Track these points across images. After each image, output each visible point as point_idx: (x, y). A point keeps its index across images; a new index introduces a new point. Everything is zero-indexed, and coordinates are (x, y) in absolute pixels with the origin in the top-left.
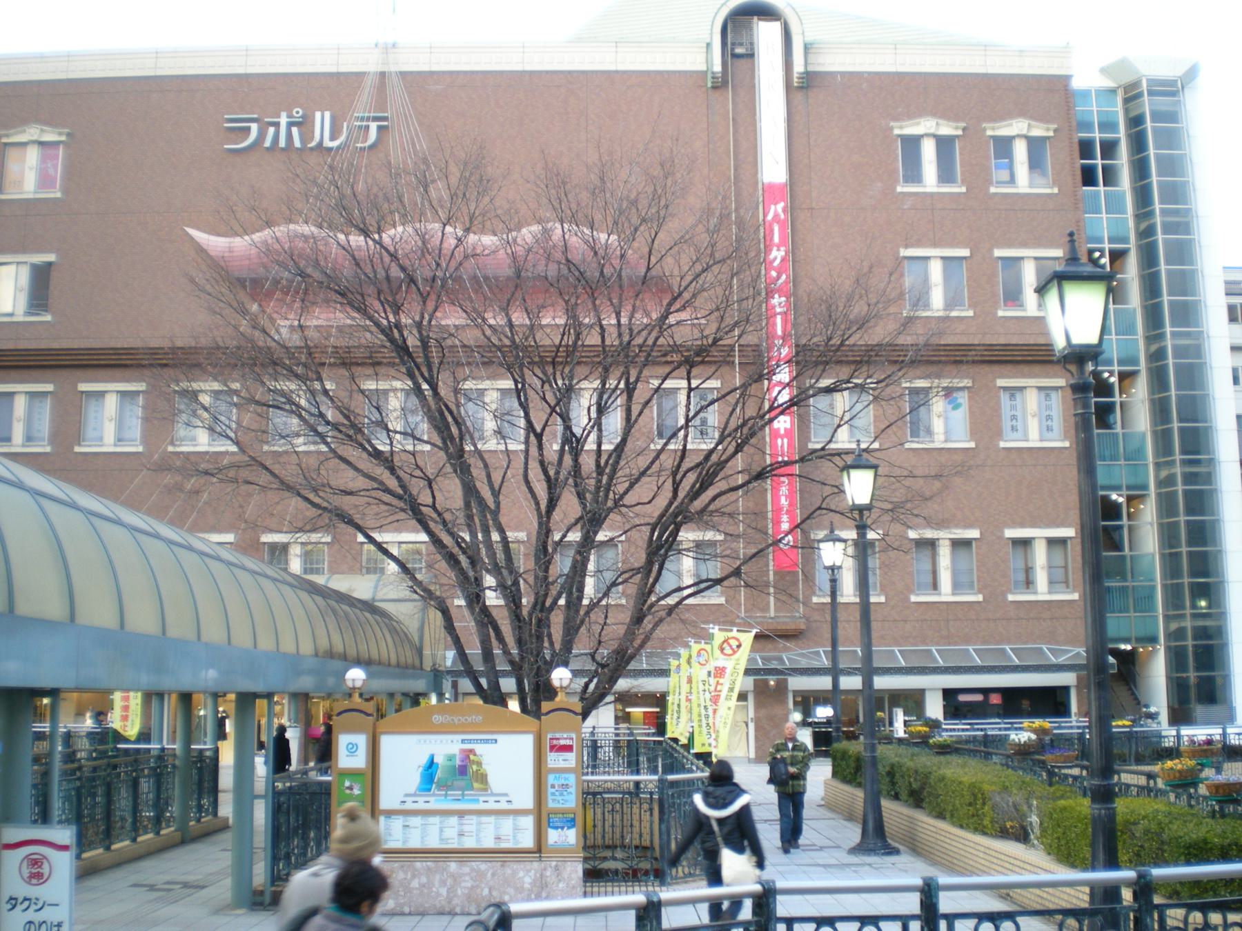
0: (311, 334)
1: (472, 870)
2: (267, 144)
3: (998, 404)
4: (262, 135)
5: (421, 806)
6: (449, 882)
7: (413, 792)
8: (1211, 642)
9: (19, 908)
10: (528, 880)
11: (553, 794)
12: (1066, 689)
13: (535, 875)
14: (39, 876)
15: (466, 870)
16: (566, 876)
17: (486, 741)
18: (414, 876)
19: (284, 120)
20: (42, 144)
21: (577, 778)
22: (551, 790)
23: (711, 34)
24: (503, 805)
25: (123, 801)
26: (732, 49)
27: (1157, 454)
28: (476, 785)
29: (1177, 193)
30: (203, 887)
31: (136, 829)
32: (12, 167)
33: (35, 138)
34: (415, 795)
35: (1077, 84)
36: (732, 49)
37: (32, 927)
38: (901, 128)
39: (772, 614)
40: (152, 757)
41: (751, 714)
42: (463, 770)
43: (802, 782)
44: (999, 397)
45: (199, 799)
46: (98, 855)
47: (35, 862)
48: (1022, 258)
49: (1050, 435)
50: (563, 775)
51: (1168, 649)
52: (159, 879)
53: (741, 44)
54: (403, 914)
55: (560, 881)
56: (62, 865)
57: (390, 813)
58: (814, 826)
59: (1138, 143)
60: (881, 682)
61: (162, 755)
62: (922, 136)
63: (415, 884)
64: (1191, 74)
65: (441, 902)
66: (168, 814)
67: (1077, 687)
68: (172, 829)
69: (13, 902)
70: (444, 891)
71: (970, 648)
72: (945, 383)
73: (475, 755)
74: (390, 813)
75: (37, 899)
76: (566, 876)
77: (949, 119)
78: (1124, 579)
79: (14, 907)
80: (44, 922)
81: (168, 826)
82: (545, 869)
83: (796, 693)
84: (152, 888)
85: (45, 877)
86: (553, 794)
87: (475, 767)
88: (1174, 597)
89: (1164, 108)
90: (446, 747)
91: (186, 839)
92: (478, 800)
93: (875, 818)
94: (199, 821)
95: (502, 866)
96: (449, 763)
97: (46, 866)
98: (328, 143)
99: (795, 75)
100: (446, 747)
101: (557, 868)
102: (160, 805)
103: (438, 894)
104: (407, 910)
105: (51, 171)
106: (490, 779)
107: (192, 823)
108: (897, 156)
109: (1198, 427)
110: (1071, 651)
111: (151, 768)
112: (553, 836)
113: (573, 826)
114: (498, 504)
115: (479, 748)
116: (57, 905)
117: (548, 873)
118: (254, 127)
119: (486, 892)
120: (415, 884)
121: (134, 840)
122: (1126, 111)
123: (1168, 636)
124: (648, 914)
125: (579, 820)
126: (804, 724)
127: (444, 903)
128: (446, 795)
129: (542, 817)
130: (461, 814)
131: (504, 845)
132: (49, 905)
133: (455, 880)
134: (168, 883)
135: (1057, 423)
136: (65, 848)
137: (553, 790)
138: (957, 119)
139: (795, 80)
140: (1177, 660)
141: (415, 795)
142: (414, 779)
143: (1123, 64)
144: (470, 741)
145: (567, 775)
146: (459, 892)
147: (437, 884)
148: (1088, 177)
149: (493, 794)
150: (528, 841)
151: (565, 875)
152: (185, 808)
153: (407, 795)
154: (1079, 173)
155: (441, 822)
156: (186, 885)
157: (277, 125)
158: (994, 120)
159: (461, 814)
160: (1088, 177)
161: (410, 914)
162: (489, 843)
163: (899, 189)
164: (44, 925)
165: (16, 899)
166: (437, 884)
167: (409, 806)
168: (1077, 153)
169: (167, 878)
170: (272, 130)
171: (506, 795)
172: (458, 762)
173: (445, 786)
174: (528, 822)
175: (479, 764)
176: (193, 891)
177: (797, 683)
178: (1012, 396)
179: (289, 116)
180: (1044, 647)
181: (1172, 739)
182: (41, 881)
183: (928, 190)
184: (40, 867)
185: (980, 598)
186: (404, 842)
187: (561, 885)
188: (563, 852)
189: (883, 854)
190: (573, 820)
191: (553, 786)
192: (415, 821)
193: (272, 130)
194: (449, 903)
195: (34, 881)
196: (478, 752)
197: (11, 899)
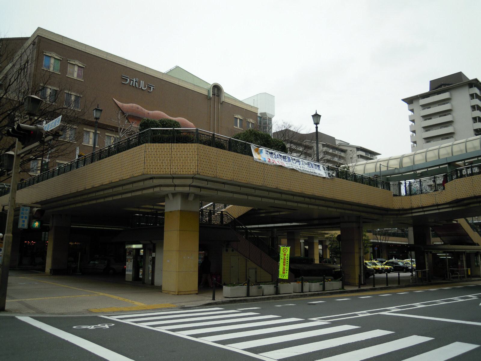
4: (130, 82)
19: (134, 80)
35: (335, 138)
43: (32, 132)
48: (90, 132)
64: (403, 100)
72: (271, 151)
74: (472, 218)
98: (143, 89)
105: (80, 74)
157: (133, 81)
170: (132, 82)
179: (136, 80)
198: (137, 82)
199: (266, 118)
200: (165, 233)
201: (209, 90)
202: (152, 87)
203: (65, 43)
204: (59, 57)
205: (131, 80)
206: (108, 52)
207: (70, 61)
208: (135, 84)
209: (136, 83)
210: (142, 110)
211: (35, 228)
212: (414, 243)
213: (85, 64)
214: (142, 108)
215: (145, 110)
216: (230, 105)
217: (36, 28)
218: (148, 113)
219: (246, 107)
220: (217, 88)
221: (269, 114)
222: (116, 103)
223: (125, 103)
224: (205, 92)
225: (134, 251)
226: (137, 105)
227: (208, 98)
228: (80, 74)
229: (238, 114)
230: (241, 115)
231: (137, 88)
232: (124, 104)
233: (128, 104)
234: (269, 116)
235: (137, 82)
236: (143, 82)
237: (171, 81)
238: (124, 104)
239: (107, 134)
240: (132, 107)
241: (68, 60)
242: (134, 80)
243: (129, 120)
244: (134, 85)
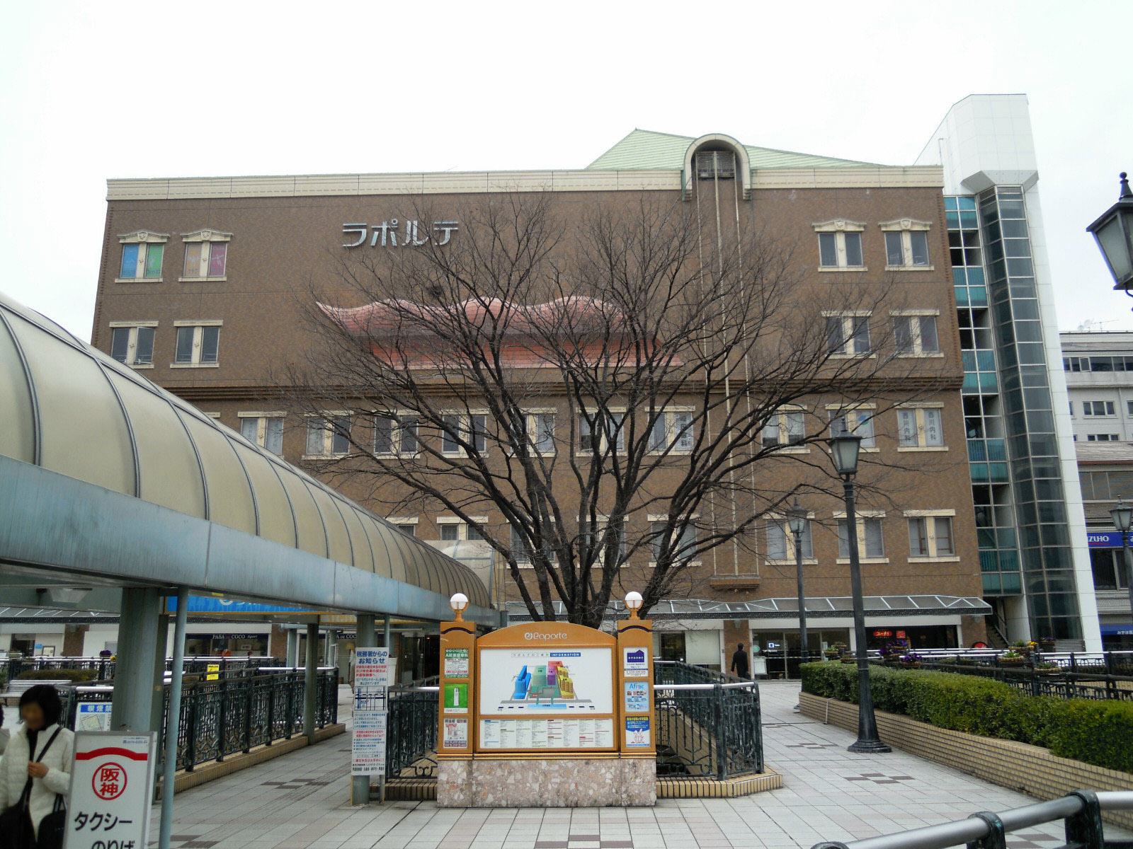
0: (398, 439)
1: (561, 767)
2: (373, 243)
3: (896, 419)
5: (516, 711)
6: (541, 778)
7: (509, 699)
8: (1061, 593)
9: (88, 826)
10: (609, 776)
11: (629, 700)
12: (954, 627)
13: (615, 771)
14: (113, 789)
15: (556, 767)
16: (642, 773)
17: (571, 655)
18: (510, 773)
19: (384, 227)
20: (212, 243)
21: (650, 688)
22: (627, 697)
23: (684, 164)
24: (587, 711)
25: (260, 712)
26: (699, 175)
27: (1013, 454)
28: (563, 693)
29: (1025, 267)
30: (326, 784)
31: (271, 734)
32: (190, 258)
33: (909, 228)
34: (510, 702)
36: (699, 175)
37: (101, 847)
38: (820, 226)
39: (737, 574)
40: (287, 675)
41: (722, 647)
42: (551, 680)
44: (896, 416)
45: (322, 710)
46: (237, 757)
47: (108, 774)
49: (933, 442)
50: (638, 684)
51: (1029, 597)
52: (287, 778)
53: (705, 171)
54: (500, 807)
55: (636, 777)
56: (139, 776)
57: (488, 718)
58: (803, 728)
59: (993, 232)
60: (811, 623)
61: (293, 675)
62: (835, 232)
63: (511, 780)
64: (1035, 178)
65: (533, 797)
66: (298, 722)
67: (962, 626)
68: (301, 734)
69: (83, 819)
70: (536, 787)
71: (882, 597)
73: (562, 666)
74: (488, 718)
75: (109, 815)
76: (642, 773)
77: (854, 220)
78: (993, 545)
79: (83, 824)
80: (115, 842)
81: (297, 732)
82: (624, 767)
83: (755, 631)
84: (281, 786)
85: (120, 790)
86: (629, 700)
87: (562, 677)
88: (1033, 559)
89: (1011, 207)
90: (537, 661)
91: (311, 741)
92: (565, 706)
93: (870, 721)
94: (321, 727)
95: (587, 763)
96: (541, 674)
97: (121, 777)
99: (744, 191)
100: (537, 661)
101: (634, 765)
102: (290, 716)
103: (532, 790)
104: (504, 803)
105: (219, 262)
106: (575, 688)
107: (316, 729)
108: (818, 246)
109: (1032, 443)
110: (956, 599)
111: (284, 685)
112: (630, 737)
113: (647, 728)
114: (549, 482)
115: (565, 661)
116: (130, 822)
117: (627, 770)
118: (364, 231)
119: (573, 786)
120: (511, 780)
121: (269, 744)
122: (982, 211)
123: (1029, 588)
124: (2, 651)
125: (652, 722)
126: (761, 654)
127: (537, 797)
128: (537, 702)
129: (620, 721)
130: (551, 718)
131: (587, 745)
132: (121, 822)
133: (546, 776)
134: (295, 781)
135: (938, 433)
136: (143, 757)
137: (630, 697)
138: (859, 219)
139: (744, 195)
140: (1038, 606)
141: (510, 702)
142: (510, 688)
143: (980, 176)
144: (558, 655)
145: (641, 684)
146: (550, 787)
147: (530, 779)
148: (956, 258)
149: (578, 701)
150: (608, 742)
151: (641, 772)
152: (311, 718)
153: (503, 702)
154: (949, 255)
155: (534, 727)
156: (311, 782)
157: (380, 230)
158: (186, 230)
159: (551, 718)
160: (956, 258)
161: (507, 807)
162: (575, 744)
163: (820, 270)
164: (114, 845)
165: (86, 816)
166: (530, 779)
167: (506, 711)
168: (947, 242)
169: (297, 776)
171: (589, 701)
172: (547, 673)
173: (537, 694)
174: (608, 725)
175: (566, 674)
176: (317, 787)
177: (755, 624)
178: (905, 415)
179: (388, 224)
180: (936, 596)
181: (1067, 661)
182: (115, 794)
183: (841, 270)
184: (115, 778)
185: (887, 560)
186: (502, 741)
187: (638, 780)
188: (639, 753)
189: (879, 751)
190: (648, 722)
191: (629, 694)
192: (511, 725)
193: (376, 233)
194: (541, 797)
195: (107, 795)
196: (564, 664)
197: (81, 815)
202: (448, 230)
203: (176, 193)
204: (158, 236)
208: (389, 238)
213: (229, 231)
216: (793, 196)
219: (900, 178)
224: (668, 181)
229: (828, 217)
239: (240, 414)
241: (880, 226)
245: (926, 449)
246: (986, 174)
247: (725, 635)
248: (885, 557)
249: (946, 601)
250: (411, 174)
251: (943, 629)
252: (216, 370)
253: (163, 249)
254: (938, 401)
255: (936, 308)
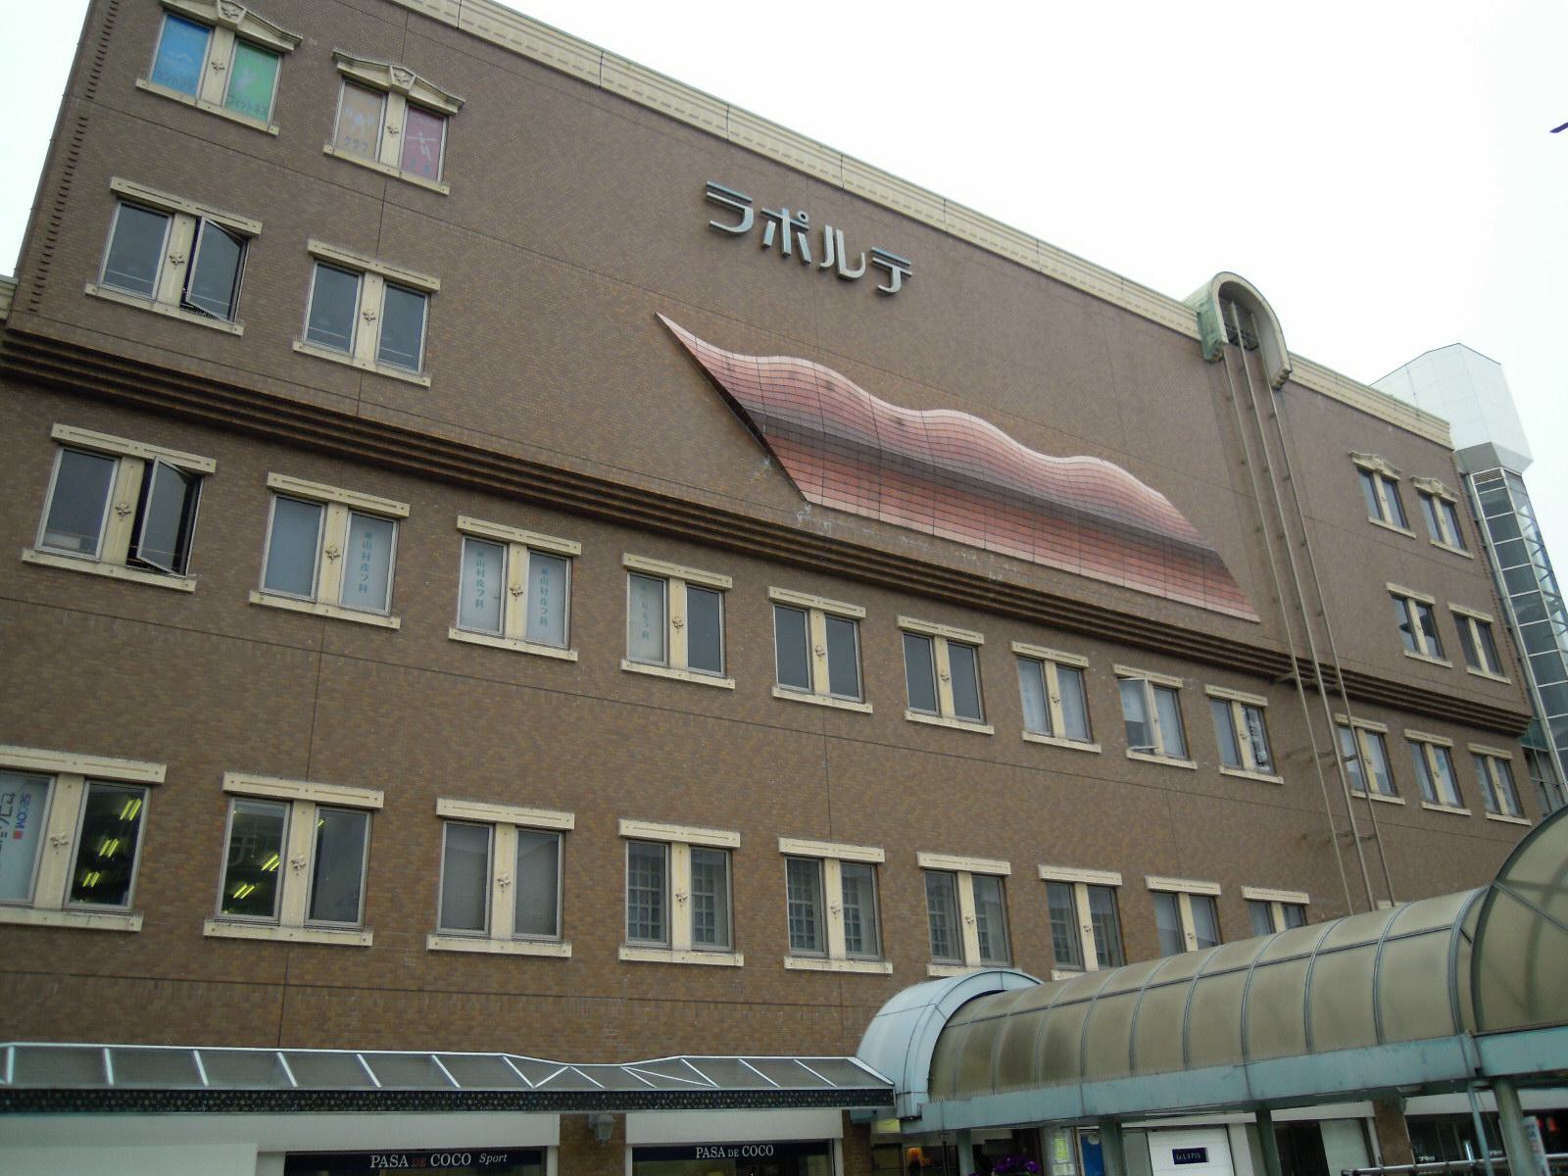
98: (844, 271)
105: (425, 151)
110: (799, 1060)
157: (779, 221)
198: (803, 230)
199: (1498, 473)
200: (1270, 1097)
201: (1199, 314)
202: (896, 271)
205: (763, 217)
206: (1338, 371)
207: (350, 62)
208: (795, 243)
209: (801, 236)
210: (852, 396)
211: (326, 1169)
212: (267, 475)
214: (851, 384)
215: (875, 399)
217: (1445, 418)
218: (900, 422)
219: (1031, 255)
220: (1236, 297)
221: (1505, 450)
222: (682, 348)
223: (743, 351)
224: (1183, 321)
225: (639, 1164)
226: (819, 367)
227: (1208, 356)
228: (425, 151)
230: (1383, 454)
231: (805, 263)
232: (739, 358)
233: (763, 360)
234: (1508, 463)
235: (803, 230)
236: (840, 234)
237: (1420, 429)
238: (737, 356)
239: (465, 523)
240: (793, 375)
242: (787, 220)
243: (785, 462)
244: (787, 247)
245: (521, 647)
246: (1498, 452)
247: (560, 1161)
248: (732, 952)
249: (535, 1072)
250: (1059, 250)
251: (1082, 1138)
252: (420, 394)
253: (277, 66)
254: (1449, 736)
255: (1434, 594)
